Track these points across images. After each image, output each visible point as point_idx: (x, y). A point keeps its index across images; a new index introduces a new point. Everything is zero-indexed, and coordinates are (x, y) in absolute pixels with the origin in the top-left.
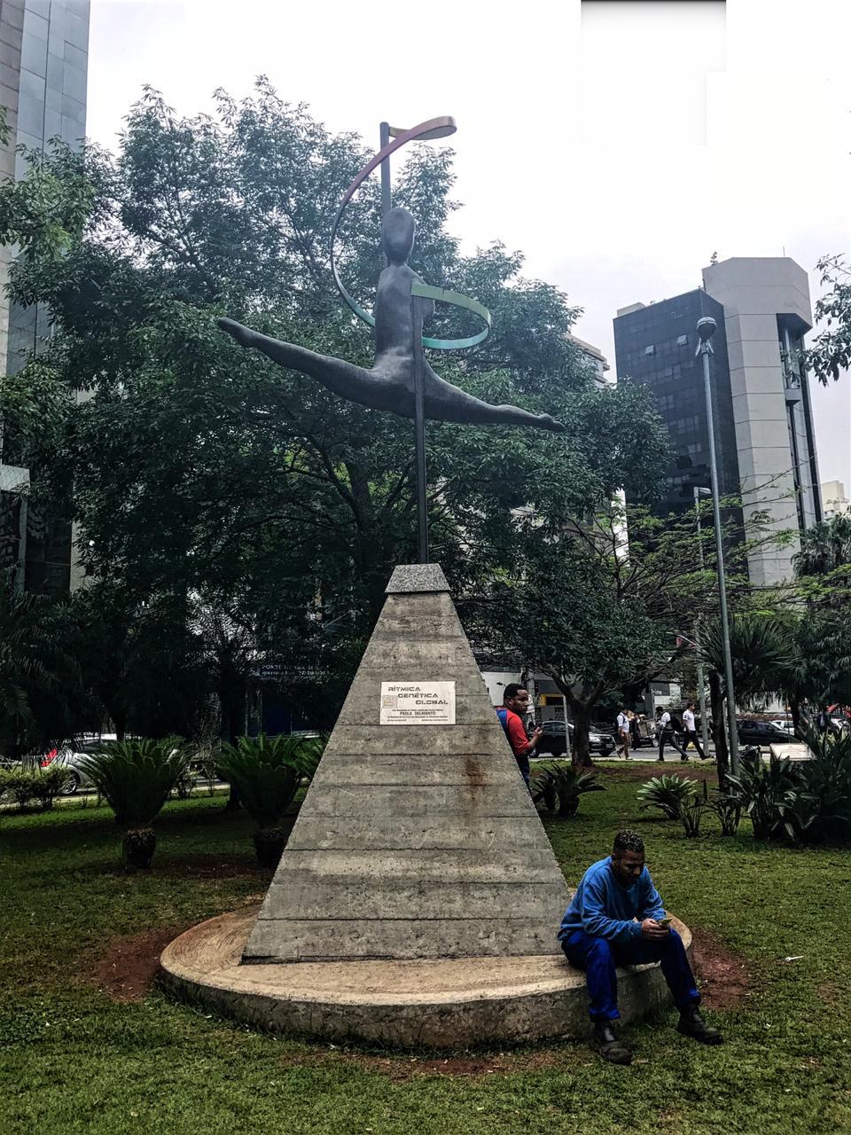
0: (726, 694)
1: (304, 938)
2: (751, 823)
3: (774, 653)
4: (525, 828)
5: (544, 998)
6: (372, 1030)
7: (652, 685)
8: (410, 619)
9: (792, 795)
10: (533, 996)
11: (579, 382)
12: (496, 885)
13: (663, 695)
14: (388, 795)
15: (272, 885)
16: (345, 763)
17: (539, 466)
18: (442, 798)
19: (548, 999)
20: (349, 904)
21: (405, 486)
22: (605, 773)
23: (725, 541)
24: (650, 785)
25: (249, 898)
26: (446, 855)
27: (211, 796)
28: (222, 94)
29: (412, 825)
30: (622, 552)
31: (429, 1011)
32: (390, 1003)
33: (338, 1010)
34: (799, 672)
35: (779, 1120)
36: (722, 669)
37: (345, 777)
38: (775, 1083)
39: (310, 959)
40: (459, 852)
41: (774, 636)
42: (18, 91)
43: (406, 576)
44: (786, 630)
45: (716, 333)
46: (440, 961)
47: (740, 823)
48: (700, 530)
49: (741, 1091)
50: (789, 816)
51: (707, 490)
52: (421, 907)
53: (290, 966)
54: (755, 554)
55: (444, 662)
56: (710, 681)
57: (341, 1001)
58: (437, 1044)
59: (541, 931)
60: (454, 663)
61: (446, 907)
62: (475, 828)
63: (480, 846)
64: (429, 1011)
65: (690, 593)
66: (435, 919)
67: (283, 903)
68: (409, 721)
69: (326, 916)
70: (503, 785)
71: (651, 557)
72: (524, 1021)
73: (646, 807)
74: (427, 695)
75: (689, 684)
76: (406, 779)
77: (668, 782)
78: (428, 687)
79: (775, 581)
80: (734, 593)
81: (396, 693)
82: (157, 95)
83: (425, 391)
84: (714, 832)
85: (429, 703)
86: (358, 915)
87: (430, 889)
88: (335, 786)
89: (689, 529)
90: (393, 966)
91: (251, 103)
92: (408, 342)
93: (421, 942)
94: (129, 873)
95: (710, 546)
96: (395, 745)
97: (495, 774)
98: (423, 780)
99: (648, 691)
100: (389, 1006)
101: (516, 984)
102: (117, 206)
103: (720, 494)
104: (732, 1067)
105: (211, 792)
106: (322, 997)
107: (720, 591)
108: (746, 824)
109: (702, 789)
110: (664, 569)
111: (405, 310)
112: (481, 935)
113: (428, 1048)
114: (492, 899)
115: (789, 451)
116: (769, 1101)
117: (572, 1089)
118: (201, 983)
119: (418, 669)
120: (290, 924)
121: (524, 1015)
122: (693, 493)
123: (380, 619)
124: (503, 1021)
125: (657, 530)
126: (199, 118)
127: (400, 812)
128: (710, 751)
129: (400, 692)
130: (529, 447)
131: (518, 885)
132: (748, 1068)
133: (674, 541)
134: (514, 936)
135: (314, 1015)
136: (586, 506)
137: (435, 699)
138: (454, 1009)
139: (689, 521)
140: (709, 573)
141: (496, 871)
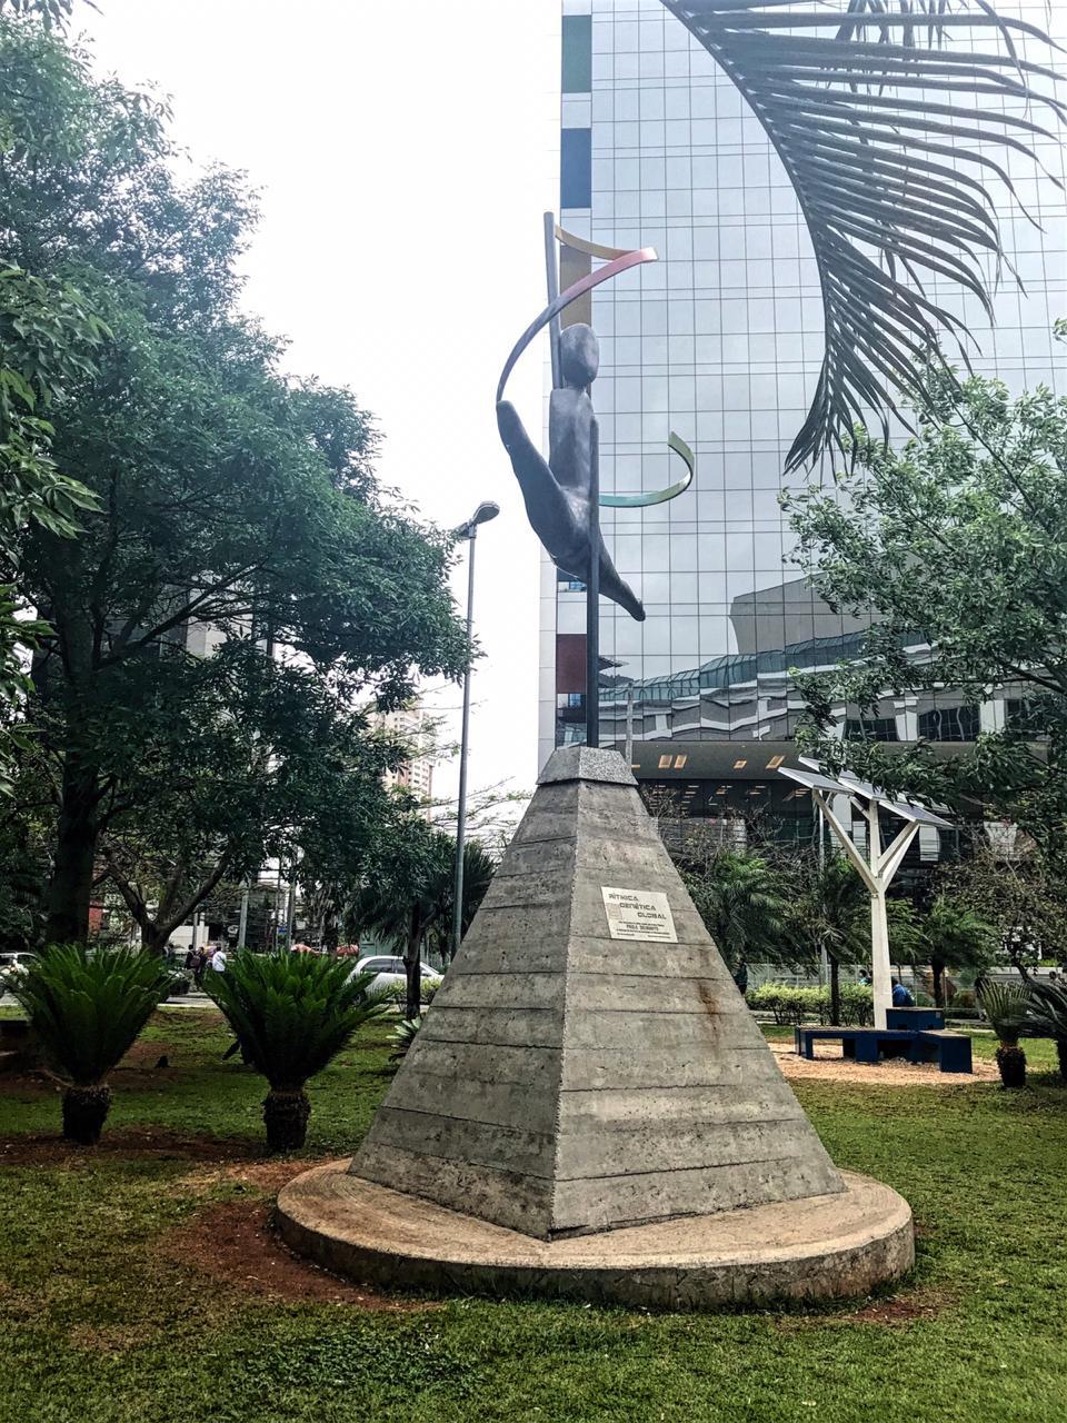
6: (798, 1289)
12: (757, 1124)
14: (641, 1023)
20: (638, 1153)
33: (765, 1270)
39: (620, 1225)
59: (805, 1170)
66: (720, 1166)
67: (576, 1159)
69: (622, 1171)
78: (644, 897)
81: (617, 901)
93: (714, 1192)
100: (812, 1258)
114: (758, 1139)
120: (589, 1185)
131: (774, 1123)
137: (653, 912)
141: (751, 1109)
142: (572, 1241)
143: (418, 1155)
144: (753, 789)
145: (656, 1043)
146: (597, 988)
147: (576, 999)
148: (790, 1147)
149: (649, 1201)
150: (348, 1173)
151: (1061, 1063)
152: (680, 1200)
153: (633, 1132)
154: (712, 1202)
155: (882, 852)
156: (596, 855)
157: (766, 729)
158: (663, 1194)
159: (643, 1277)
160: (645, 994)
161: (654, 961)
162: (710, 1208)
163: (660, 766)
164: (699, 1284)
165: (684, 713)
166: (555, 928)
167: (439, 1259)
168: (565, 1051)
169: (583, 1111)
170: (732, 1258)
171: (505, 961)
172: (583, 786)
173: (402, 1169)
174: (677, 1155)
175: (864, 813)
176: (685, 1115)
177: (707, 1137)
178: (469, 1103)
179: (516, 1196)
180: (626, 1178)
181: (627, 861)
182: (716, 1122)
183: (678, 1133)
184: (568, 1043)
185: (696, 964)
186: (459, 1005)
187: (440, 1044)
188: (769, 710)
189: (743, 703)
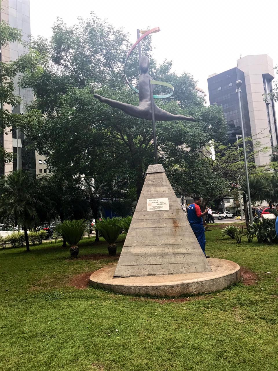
0: (248, 200)
1: (131, 271)
2: (257, 239)
3: (263, 186)
4: (191, 238)
5: (199, 283)
6: (153, 293)
7: (224, 199)
8: (154, 180)
9: (269, 229)
10: (196, 282)
11: (199, 104)
12: (184, 254)
13: (228, 203)
14: (151, 230)
15: (120, 256)
16: (138, 222)
17: (188, 132)
18: (167, 231)
19: (200, 283)
20: (142, 260)
22: (210, 227)
23: (247, 152)
24: (225, 229)
25: (109, 264)
26: (169, 246)
27: (89, 238)
28: (80, 18)
29: (159, 238)
30: (213, 157)
31: (168, 287)
32: (157, 285)
34: (271, 193)
35: (265, 309)
36: (247, 192)
37: (139, 226)
38: (265, 301)
40: (172, 245)
41: (263, 181)
42: (8, 15)
43: (152, 168)
44: (267, 179)
45: (243, 86)
46: (169, 275)
47: (254, 239)
48: (238, 149)
49: (255, 303)
50: (269, 235)
51: (240, 136)
52: (162, 260)
53: (127, 278)
54: (256, 156)
55: (165, 192)
56: (243, 198)
57: (144, 285)
58: (171, 295)
59: (197, 266)
60: (168, 193)
61: (170, 261)
62: (176, 239)
63: (178, 243)
64: (168, 287)
65: (236, 169)
68: (156, 210)
70: (184, 226)
71: (223, 158)
72: (194, 289)
73: (224, 235)
74: (161, 202)
75: (236, 199)
76: (156, 226)
77: (231, 227)
79: (263, 164)
80: (250, 169)
81: (152, 202)
82: (61, 20)
83: (155, 112)
84: (246, 242)
85: (161, 204)
86: (145, 264)
87: (165, 256)
88: (136, 229)
89: (235, 149)
90: (156, 277)
91: (89, 19)
92: (149, 97)
93: (163, 270)
94: (72, 259)
95: (242, 154)
96: (152, 216)
97: (181, 223)
98: (161, 226)
99: (223, 202)
101: (192, 279)
102: (50, 56)
103: (245, 137)
104: (252, 298)
105: (89, 237)
106: (138, 285)
107: (246, 168)
108: (255, 239)
109: (241, 229)
110: (227, 162)
111: (148, 88)
112: (180, 268)
113: (168, 296)
115: (267, 120)
116: (262, 305)
117: (208, 304)
118: (103, 283)
119: (157, 195)
121: (194, 287)
122: (236, 137)
123: (145, 181)
124: (189, 289)
125: (225, 150)
126: (74, 26)
127: (155, 235)
128: (244, 219)
129: (152, 202)
130: (184, 126)
131: (190, 254)
132: (256, 298)
133: (230, 153)
134: (189, 268)
135: (136, 289)
136: (203, 144)
138: (175, 286)
139: (235, 146)
140: (242, 162)
141: (183, 250)
148: (195, 260)
154: (162, 272)
162: (160, 273)
164: (128, 289)
169: (128, 251)
174: (154, 261)
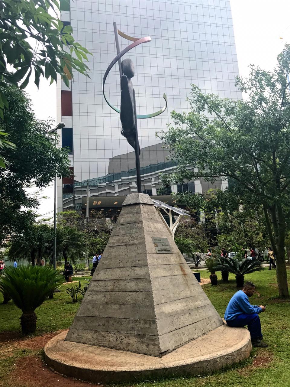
21: (261, 173)
69: (174, 329)
131: (205, 306)
142: (167, 355)
143: (96, 332)
144: (118, 209)
145: (174, 285)
146: (157, 270)
147: (153, 274)
149: (183, 337)
150: (66, 340)
151: (223, 277)
152: (190, 335)
153: (174, 315)
154: (197, 334)
155: (173, 224)
156: (148, 227)
157: (118, 194)
158: (185, 334)
159: (197, 365)
160: (168, 270)
161: (168, 260)
163: (94, 204)
164: (213, 364)
165: (102, 188)
166: (140, 251)
167: (128, 370)
168: (153, 292)
170: (221, 353)
171: (121, 263)
172: (141, 205)
173: (90, 337)
174: (186, 321)
175: (168, 214)
176: (186, 307)
177: (191, 314)
178: (114, 311)
179: (143, 343)
180: (175, 331)
181: (156, 228)
182: (193, 309)
183: (185, 314)
184: (153, 289)
185: (178, 259)
186: (104, 279)
187: (98, 293)
188: (118, 189)
189: (84, 191)
